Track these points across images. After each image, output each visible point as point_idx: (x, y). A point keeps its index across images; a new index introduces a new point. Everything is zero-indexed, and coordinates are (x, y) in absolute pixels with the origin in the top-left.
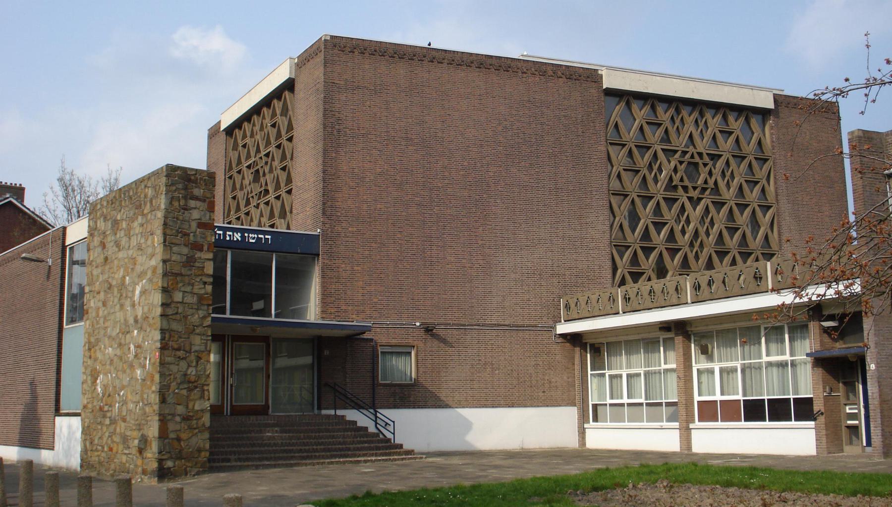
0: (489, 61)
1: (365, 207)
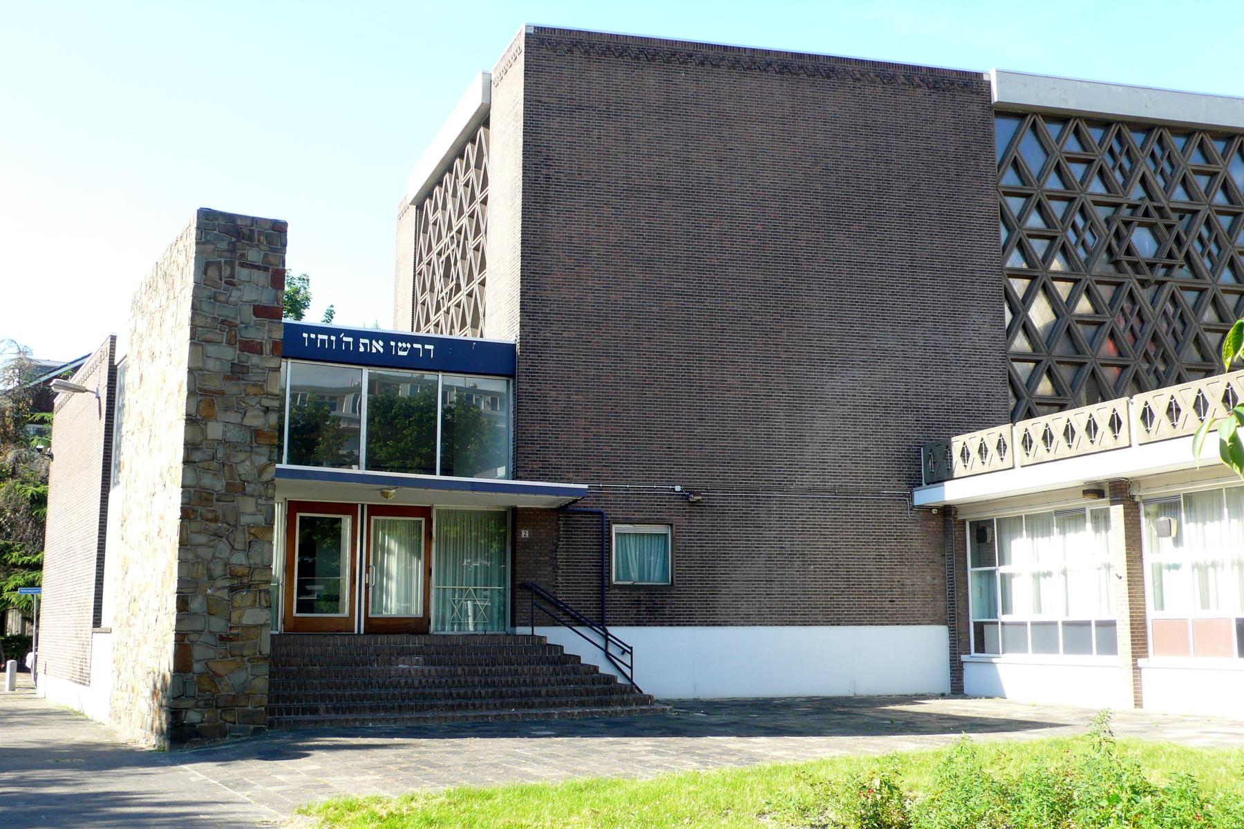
0: (798, 62)
1: (590, 298)
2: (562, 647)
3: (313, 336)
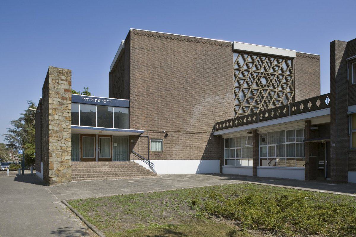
0: (315, 57)
2: (139, 164)
3: (84, 98)
